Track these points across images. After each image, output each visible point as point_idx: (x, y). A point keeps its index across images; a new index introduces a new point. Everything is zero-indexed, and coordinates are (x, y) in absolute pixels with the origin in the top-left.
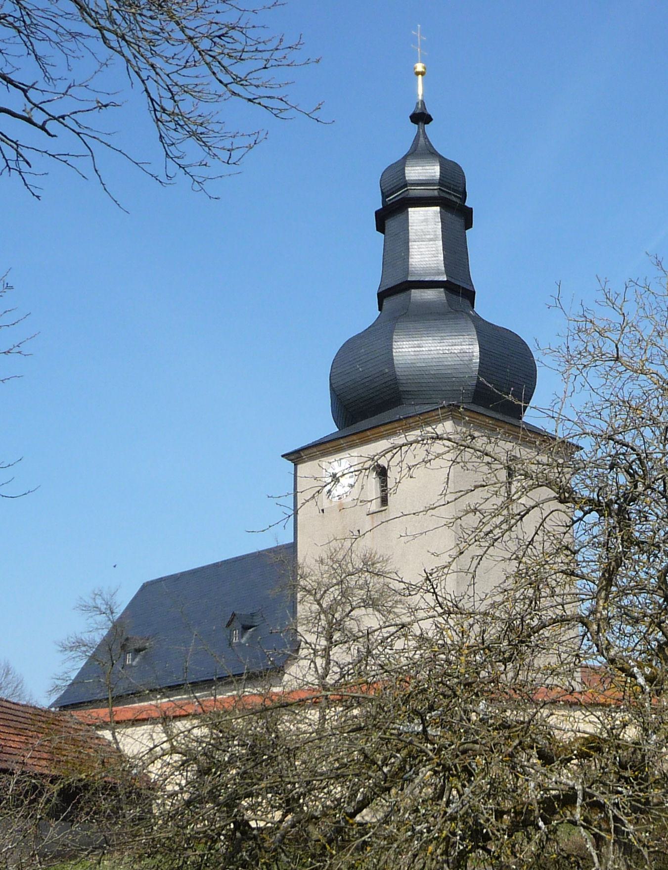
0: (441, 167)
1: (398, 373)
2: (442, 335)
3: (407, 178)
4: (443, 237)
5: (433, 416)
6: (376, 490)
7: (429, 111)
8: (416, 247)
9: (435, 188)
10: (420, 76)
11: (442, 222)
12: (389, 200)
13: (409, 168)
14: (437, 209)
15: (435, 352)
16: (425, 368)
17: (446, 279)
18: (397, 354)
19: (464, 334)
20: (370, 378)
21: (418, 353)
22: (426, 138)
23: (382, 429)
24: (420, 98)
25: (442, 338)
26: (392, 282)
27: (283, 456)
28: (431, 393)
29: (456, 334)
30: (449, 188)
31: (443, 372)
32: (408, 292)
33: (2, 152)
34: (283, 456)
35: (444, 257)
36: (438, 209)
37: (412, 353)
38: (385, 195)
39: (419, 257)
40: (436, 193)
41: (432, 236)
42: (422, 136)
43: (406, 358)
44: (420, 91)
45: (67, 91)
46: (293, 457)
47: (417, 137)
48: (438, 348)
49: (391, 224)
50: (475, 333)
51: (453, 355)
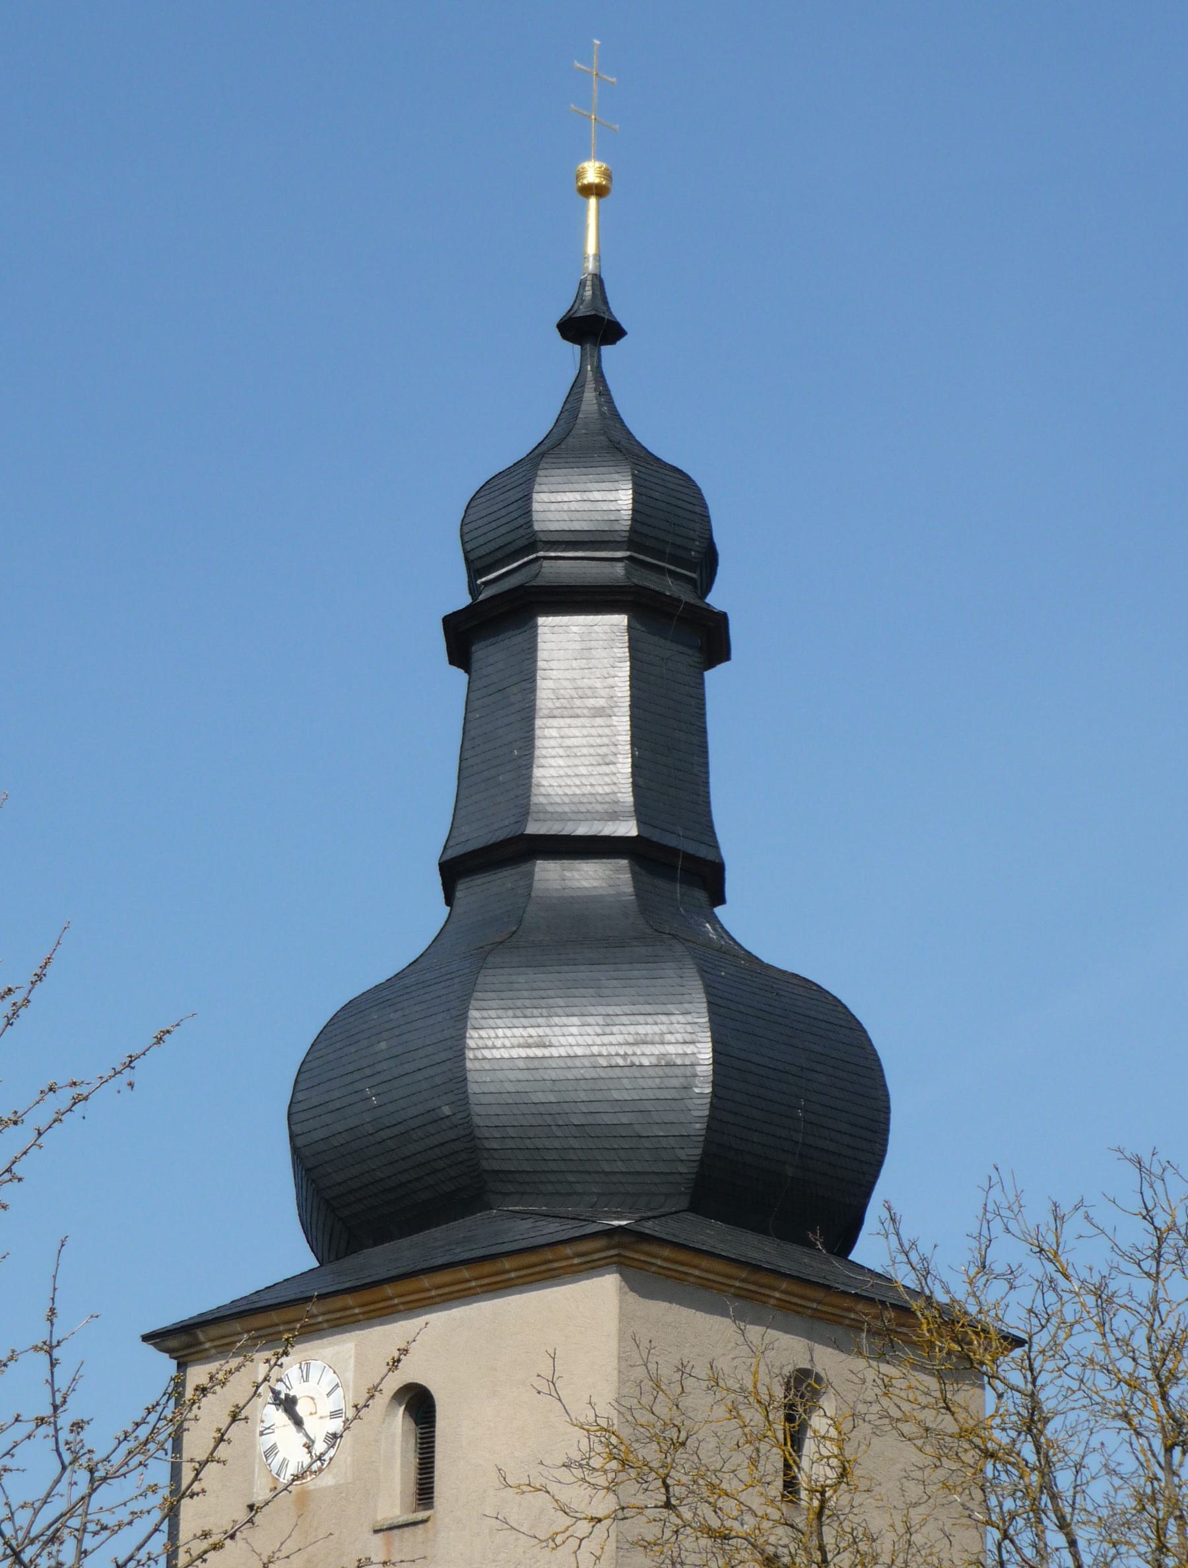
0: (635, 492)
1: (477, 1120)
2: (610, 1010)
3: (537, 527)
4: (633, 706)
5: (568, 1258)
6: (403, 1456)
7: (620, 311)
8: (554, 732)
9: (619, 554)
10: (593, 201)
11: (633, 659)
12: (486, 584)
13: (544, 497)
14: (621, 620)
15: (586, 1062)
16: (556, 1109)
17: (634, 832)
18: (477, 1065)
19: (671, 1008)
20: (401, 1128)
21: (536, 1064)
22: (604, 392)
23: (426, 1282)
24: (591, 266)
25: (609, 1021)
26: (479, 837)
27: (146, 1338)
28: (571, 1178)
29: (648, 1008)
30: (660, 555)
31: (607, 1119)
32: (524, 868)
33: (3, 1488)
34: (146, 1338)
35: (634, 765)
36: (622, 620)
37: (521, 1064)
38: (476, 567)
39: (561, 762)
40: (619, 569)
41: (602, 702)
42: (590, 385)
43: (500, 1076)
44: (591, 248)
45: (62, 1463)
46: (173, 1343)
47: (577, 386)
48: (595, 1050)
49: (483, 653)
50: (703, 1007)
51: (636, 1072)
